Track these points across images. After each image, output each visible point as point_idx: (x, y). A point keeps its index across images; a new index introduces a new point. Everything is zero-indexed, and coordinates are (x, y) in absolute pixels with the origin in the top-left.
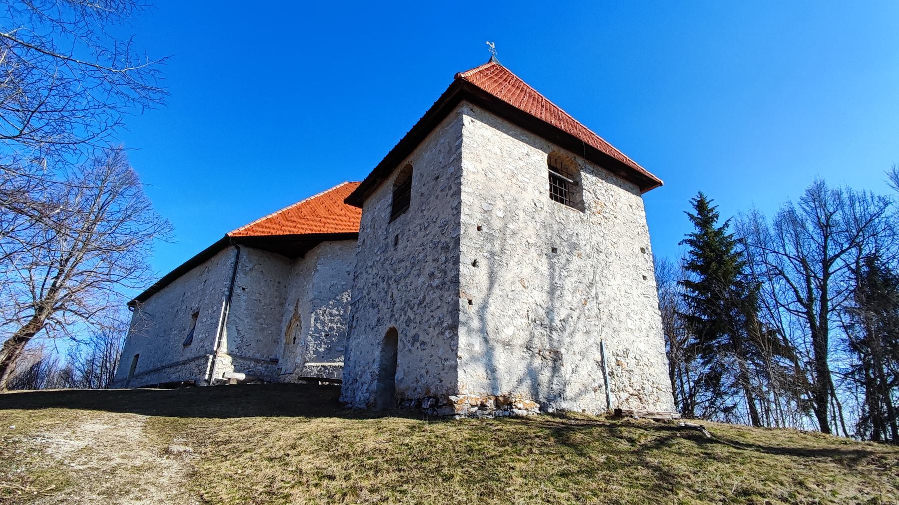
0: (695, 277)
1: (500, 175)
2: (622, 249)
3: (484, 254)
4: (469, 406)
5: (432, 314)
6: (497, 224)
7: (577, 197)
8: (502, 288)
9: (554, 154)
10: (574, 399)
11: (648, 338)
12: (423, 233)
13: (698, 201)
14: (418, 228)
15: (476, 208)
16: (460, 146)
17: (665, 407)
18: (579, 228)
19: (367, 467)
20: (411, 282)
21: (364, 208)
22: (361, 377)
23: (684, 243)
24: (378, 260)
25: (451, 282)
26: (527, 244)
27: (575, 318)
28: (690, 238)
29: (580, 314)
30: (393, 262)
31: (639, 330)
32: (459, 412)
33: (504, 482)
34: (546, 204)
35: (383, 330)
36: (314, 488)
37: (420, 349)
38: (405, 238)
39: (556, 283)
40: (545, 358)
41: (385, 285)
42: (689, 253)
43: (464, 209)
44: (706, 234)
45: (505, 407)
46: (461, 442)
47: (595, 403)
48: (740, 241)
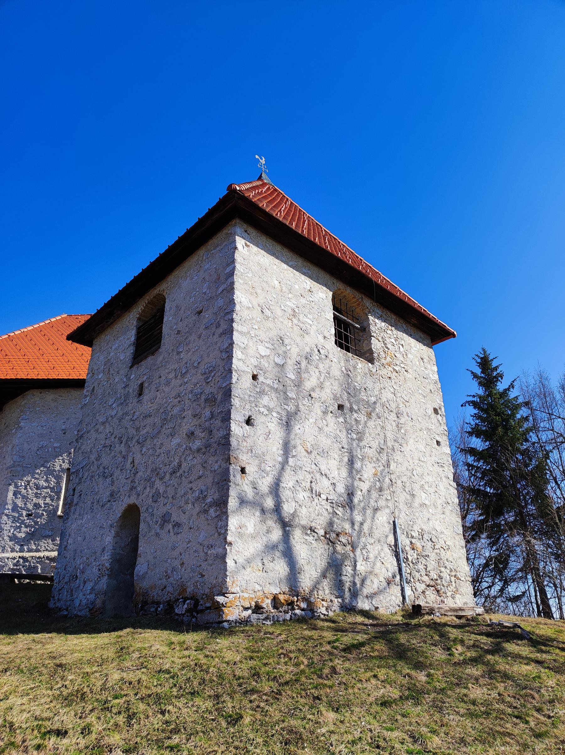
0: (477, 443)
1: (279, 313)
3: (260, 409)
4: (241, 608)
5: (191, 485)
7: (364, 345)
9: (339, 292)
11: (444, 516)
12: (179, 382)
13: (482, 358)
14: (172, 375)
16: (231, 274)
19: (114, 710)
20: (162, 444)
21: (94, 347)
22: (83, 572)
23: (467, 405)
24: (113, 414)
28: (474, 399)
30: (135, 417)
31: (434, 505)
33: (312, 721)
35: (119, 508)
37: (172, 534)
38: (153, 387)
41: (122, 447)
42: (471, 416)
43: (237, 354)
44: (490, 395)
46: (241, 662)
47: (389, 598)
48: (527, 404)
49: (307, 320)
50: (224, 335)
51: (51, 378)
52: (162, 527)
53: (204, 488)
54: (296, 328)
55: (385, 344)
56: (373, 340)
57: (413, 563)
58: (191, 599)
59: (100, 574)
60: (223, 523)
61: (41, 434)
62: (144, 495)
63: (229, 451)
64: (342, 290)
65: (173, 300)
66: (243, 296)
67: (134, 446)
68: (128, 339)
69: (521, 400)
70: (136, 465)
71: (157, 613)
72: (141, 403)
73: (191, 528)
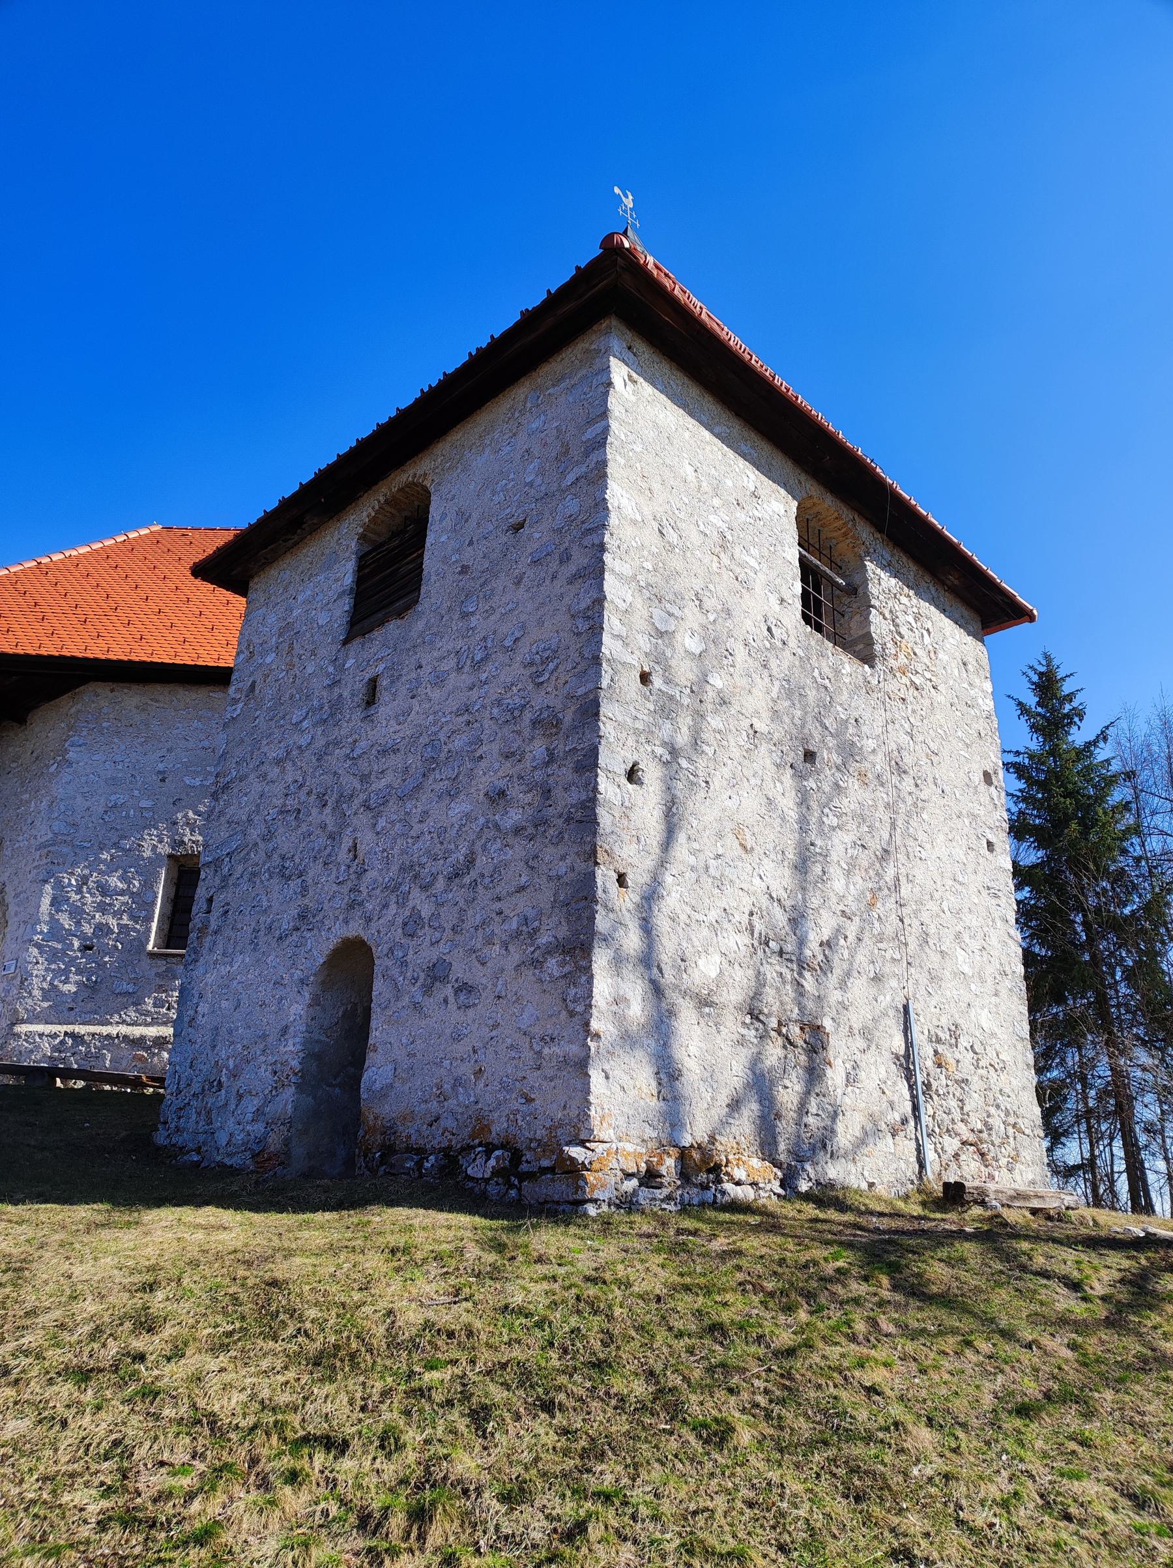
1: (695, 538)
2: (947, 772)
4: (619, 1173)
5: (497, 906)
6: (685, 672)
8: (696, 845)
10: (852, 1154)
11: (998, 1000)
12: (466, 679)
13: (1041, 674)
14: (451, 663)
15: (639, 621)
16: (600, 442)
17: (1030, 1177)
18: (862, 706)
19: (438, 1397)
20: (426, 813)
21: (252, 595)
24: (303, 742)
25: (568, 820)
26: (751, 732)
27: (852, 938)
28: (1017, 759)
29: (862, 930)
30: (358, 752)
31: (980, 977)
32: (595, 1196)
34: (792, 632)
36: (288, 1490)
37: (452, 1006)
38: (403, 690)
39: (812, 844)
40: (791, 1044)
43: (612, 622)
44: (1054, 752)
45: (703, 1177)
47: (895, 1166)
48: (1130, 775)
49: (748, 559)
50: (580, 580)
51: (137, 659)
52: (428, 990)
53: (531, 913)
54: (727, 575)
55: (896, 626)
56: (874, 616)
57: (939, 1095)
58: (503, 1146)
59: (276, 1082)
60: (580, 991)
61: (113, 779)
62: (381, 921)
63: (595, 837)
64: (815, 500)
65: (449, 496)
66: (624, 493)
67: (355, 814)
68: (337, 580)
69: (1115, 767)
70: (361, 856)
71: (421, 1172)
72: (372, 721)
73: (499, 997)
